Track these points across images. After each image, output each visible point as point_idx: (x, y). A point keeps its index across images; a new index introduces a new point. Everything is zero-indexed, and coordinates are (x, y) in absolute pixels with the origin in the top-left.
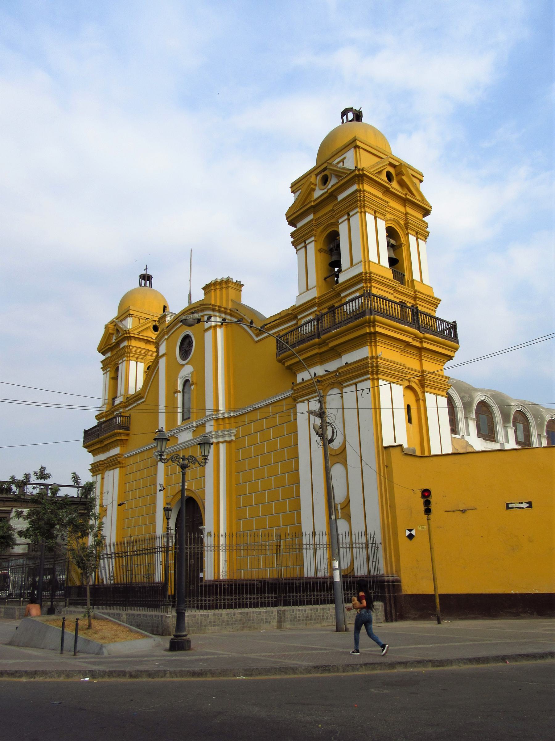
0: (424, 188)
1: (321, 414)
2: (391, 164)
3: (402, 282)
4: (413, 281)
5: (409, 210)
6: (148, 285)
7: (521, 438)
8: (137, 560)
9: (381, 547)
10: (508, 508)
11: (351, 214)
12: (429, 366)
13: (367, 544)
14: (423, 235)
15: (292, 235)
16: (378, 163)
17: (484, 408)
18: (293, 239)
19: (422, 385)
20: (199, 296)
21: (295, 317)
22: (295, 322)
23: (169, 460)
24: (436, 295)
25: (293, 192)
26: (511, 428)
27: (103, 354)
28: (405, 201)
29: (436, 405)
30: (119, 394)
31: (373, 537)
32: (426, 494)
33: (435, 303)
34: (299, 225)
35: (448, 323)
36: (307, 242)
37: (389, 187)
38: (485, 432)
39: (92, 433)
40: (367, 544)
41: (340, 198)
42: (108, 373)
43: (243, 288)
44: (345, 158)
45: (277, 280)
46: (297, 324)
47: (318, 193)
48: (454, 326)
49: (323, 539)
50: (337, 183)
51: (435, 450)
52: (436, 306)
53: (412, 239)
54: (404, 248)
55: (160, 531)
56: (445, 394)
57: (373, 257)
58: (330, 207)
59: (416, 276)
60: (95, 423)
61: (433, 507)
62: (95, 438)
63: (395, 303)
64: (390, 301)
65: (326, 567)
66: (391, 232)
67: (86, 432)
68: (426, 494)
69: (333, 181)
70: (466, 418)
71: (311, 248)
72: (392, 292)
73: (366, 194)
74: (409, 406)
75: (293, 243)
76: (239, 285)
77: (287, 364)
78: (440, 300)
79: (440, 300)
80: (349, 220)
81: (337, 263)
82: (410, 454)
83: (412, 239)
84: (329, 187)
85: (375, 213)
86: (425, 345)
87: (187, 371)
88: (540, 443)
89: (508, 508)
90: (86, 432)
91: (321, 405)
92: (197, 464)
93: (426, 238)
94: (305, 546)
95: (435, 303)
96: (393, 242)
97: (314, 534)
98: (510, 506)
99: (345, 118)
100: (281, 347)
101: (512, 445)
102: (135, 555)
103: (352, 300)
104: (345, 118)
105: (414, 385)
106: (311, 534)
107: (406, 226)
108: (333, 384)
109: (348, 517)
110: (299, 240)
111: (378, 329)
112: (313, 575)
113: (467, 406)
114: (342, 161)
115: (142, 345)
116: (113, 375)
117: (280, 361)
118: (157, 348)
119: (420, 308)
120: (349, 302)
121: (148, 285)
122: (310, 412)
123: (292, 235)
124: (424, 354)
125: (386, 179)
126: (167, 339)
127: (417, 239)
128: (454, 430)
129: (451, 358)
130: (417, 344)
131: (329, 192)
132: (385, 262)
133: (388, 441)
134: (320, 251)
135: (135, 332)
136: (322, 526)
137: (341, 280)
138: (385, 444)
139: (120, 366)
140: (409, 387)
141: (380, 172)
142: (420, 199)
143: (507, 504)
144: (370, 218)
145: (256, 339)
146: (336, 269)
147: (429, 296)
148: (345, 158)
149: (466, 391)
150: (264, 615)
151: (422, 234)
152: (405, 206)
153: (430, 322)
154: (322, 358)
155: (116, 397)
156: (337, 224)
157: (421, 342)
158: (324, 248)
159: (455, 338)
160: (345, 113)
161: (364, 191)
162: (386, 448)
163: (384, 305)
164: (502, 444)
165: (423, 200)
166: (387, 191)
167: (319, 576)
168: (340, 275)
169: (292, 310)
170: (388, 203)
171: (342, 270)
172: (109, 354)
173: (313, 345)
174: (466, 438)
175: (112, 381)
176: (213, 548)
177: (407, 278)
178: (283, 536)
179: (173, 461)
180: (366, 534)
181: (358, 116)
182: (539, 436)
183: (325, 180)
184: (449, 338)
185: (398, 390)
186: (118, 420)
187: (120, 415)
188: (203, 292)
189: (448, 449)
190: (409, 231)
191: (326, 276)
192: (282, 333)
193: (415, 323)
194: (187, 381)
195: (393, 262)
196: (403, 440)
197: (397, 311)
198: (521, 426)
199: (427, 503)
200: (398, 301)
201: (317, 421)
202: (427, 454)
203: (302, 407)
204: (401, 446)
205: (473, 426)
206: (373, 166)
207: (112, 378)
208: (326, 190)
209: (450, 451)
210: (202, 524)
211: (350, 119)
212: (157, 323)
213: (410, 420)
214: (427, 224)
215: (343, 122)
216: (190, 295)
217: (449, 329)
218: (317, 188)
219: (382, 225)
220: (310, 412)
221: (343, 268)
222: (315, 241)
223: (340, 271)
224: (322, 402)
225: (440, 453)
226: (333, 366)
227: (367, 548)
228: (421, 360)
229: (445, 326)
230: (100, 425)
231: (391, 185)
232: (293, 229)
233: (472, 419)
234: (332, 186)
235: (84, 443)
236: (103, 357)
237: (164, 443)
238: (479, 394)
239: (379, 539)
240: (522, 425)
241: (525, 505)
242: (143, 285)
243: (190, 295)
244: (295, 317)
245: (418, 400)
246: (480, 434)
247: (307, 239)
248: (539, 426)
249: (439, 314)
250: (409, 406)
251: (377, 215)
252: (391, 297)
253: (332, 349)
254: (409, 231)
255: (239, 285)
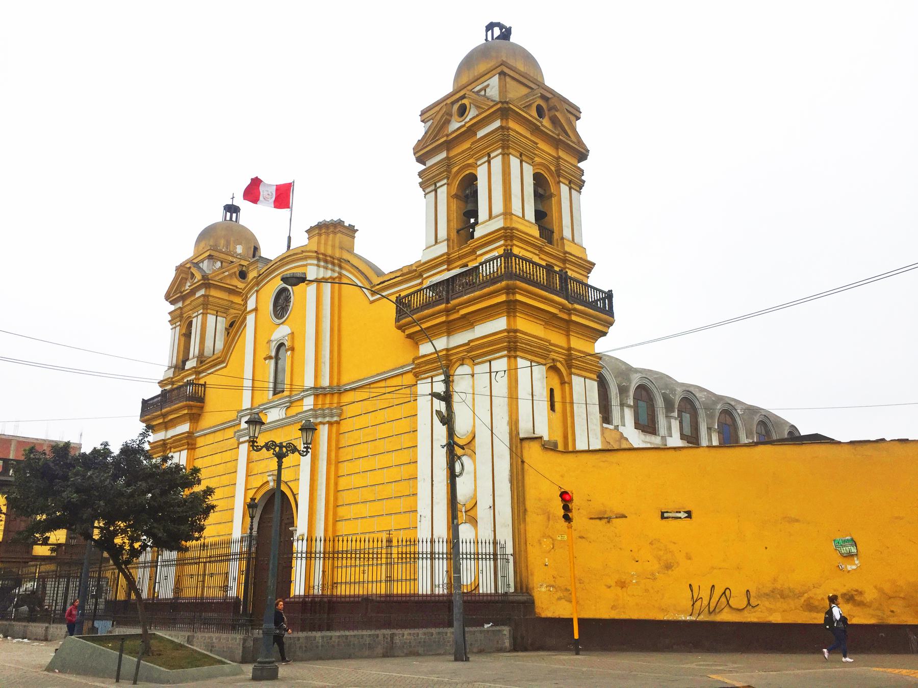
0: (580, 126)
1: (447, 398)
2: (543, 97)
3: (550, 242)
4: (562, 238)
5: (561, 154)
6: (234, 219)
7: (687, 431)
8: (211, 568)
9: (511, 559)
10: (663, 517)
11: (492, 155)
12: (578, 343)
13: (495, 554)
14: (575, 184)
15: (420, 174)
16: (526, 96)
17: (644, 393)
18: (420, 180)
19: (569, 366)
20: (301, 240)
21: (421, 275)
22: (419, 281)
23: (262, 447)
24: (590, 258)
25: (422, 121)
26: (676, 419)
27: (172, 303)
28: (556, 143)
29: (584, 389)
30: (191, 356)
31: (503, 547)
32: (565, 497)
33: (588, 267)
34: (430, 163)
35: (603, 292)
36: (438, 185)
37: (538, 124)
38: (644, 419)
39: (152, 404)
40: (495, 554)
41: (481, 134)
42: (178, 328)
43: (356, 234)
44: (488, 85)
45: (401, 231)
46: (421, 283)
47: (455, 125)
48: (609, 295)
49: (441, 548)
50: (477, 116)
51: (581, 445)
52: (589, 271)
53: (564, 189)
54: (554, 200)
55: (237, 534)
56: (595, 377)
57: (516, 208)
58: (466, 145)
59: (567, 233)
60: (158, 391)
61: (574, 514)
62: (156, 411)
63: (540, 266)
64: (534, 263)
65: (445, 581)
66: (539, 180)
67: (144, 402)
68: (565, 497)
69: (472, 113)
70: (622, 405)
71: (443, 192)
72: (537, 252)
73: (511, 133)
74: (552, 390)
75: (421, 184)
76: (351, 231)
77: (407, 332)
78: (594, 264)
79: (594, 264)
80: (489, 162)
81: (474, 213)
82: (550, 447)
83: (564, 189)
84: (467, 119)
85: (521, 155)
86: (574, 318)
87: (281, 332)
88: (710, 440)
89: (663, 517)
90: (144, 402)
91: (447, 387)
92: (297, 453)
93: (581, 188)
94: (304, 555)
95: (588, 267)
96: (540, 191)
97: (432, 541)
98: (666, 515)
99: (490, 33)
100: (400, 313)
101: (675, 440)
102: (210, 562)
103: (489, 261)
104: (490, 33)
105: (559, 365)
106: (429, 541)
107: (558, 173)
108: (463, 359)
109: (474, 521)
110: (428, 182)
111: (519, 297)
112: (429, 592)
113: (623, 390)
114: (485, 89)
115: (224, 295)
116: (184, 331)
117: (399, 328)
118: (246, 300)
119: (570, 273)
120: (485, 262)
121: (234, 219)
122: (434, 395)
123: (420, 174)
124: (572, 327)
125: (536, 115)
126: (257, 291)
127: (570, 188)
128: (606, 417)
129: (604, 334)
130: (565, 316)
131: (467, 125)
132: (530, 215)
133: (525, 429)
134: (456, 196)
135: (217, 278)
136: (442, 530)
137: (477, 235)
138: (522, 436)
139: (194, 320)
140: (553, 369)
141: (529, 106)
142: (575, 140)
143: (663, 513)
144: (514, 162)
145: (372, 299)
146: (472, 221)
147: (581, 259)
148: (488, 85)
149: (625, 371)
150: (368, 639)
151: (577, 183)
152: (557, 149)
153: (581, 290)
154: (450, 328)
155: (188, 359)
156: (475, 166)
157: (570, 314)
158: (459, 194)
159: (610, 313)
160: (490, 27)
161: (509, 129)
162: (522, 440)
163: (527, 267)
164: (664, 438)
165: (580, 142)
166: (536, 130)
167: (437, 592)
168: (477, 228)
169: (417, 267)
170: (537, 144)
171: (480, 221)
172: (180, 304)
173: (440, 312)
174: (621, 429)
175: (183, 339)
176: (299, 555)
177: (556, 236)
178: (395, 543)
179: (268, 450)
180: (495, 543)
181: (506, 34)
182: (709, 429)
183: (463, 111)
184: (602, 310)
185: (540, 371)
186: (189, 389)
187: (189, 383)
188: (306, 235)
189: (597, 444)
190: (561, 179)
191: (460, 227)
192: (403, 294)
193: (564, 291)
194: (282, 345)
195: (540, 216)
196: (543, 430)
197: (541, 275)
198: (687, 417)
199: (566, 508)
200: (544, 263)
201: (441, 406)
202: (570, 449)
203: (424, 388)
204: (541, 438)
205: (629, 415)
206: (522, 98)
207: (184, 335)
208: (463, 123)
209: (599, 447)
210: (292, 523)
211: (495, 36)
212: (244, 269)
213: (552, 408)
214: (583, 171)
215: (486, 40)
216: (289, 238)
217: (604, 299)
218: (453, 120)
219: (529, 171)
220: (434, 395)
221: (480, 220)
222: (448, 184)
223: (476, 223)
224: (448, 382)
225: (587, 448)
226: (461, 338)
227: (495, 559)
228: (568, 336)
229: (598, 296)
230: (164, 394)
231: (541, 122)
232: (422, 167)
233: (629, 406)
234: (471, 119)
235: (142, 416)
236: (172, 308)
237: (258, 427)
238: (638, 376)
239: (509, 550)
240: (688, 415)
241: (683, 515)
242: (228, 218)
243: (289, 238)
244: (421, 275)
245: (563, 383)
246: (638, 426)
247: (439, 181)
248: (710, 416)
249: (594, 279)
250: (552, 390)
251: (524, 158)
252: (536, 259)
253: (464, 316)
254: (561, 179)
255: (351, 231)
